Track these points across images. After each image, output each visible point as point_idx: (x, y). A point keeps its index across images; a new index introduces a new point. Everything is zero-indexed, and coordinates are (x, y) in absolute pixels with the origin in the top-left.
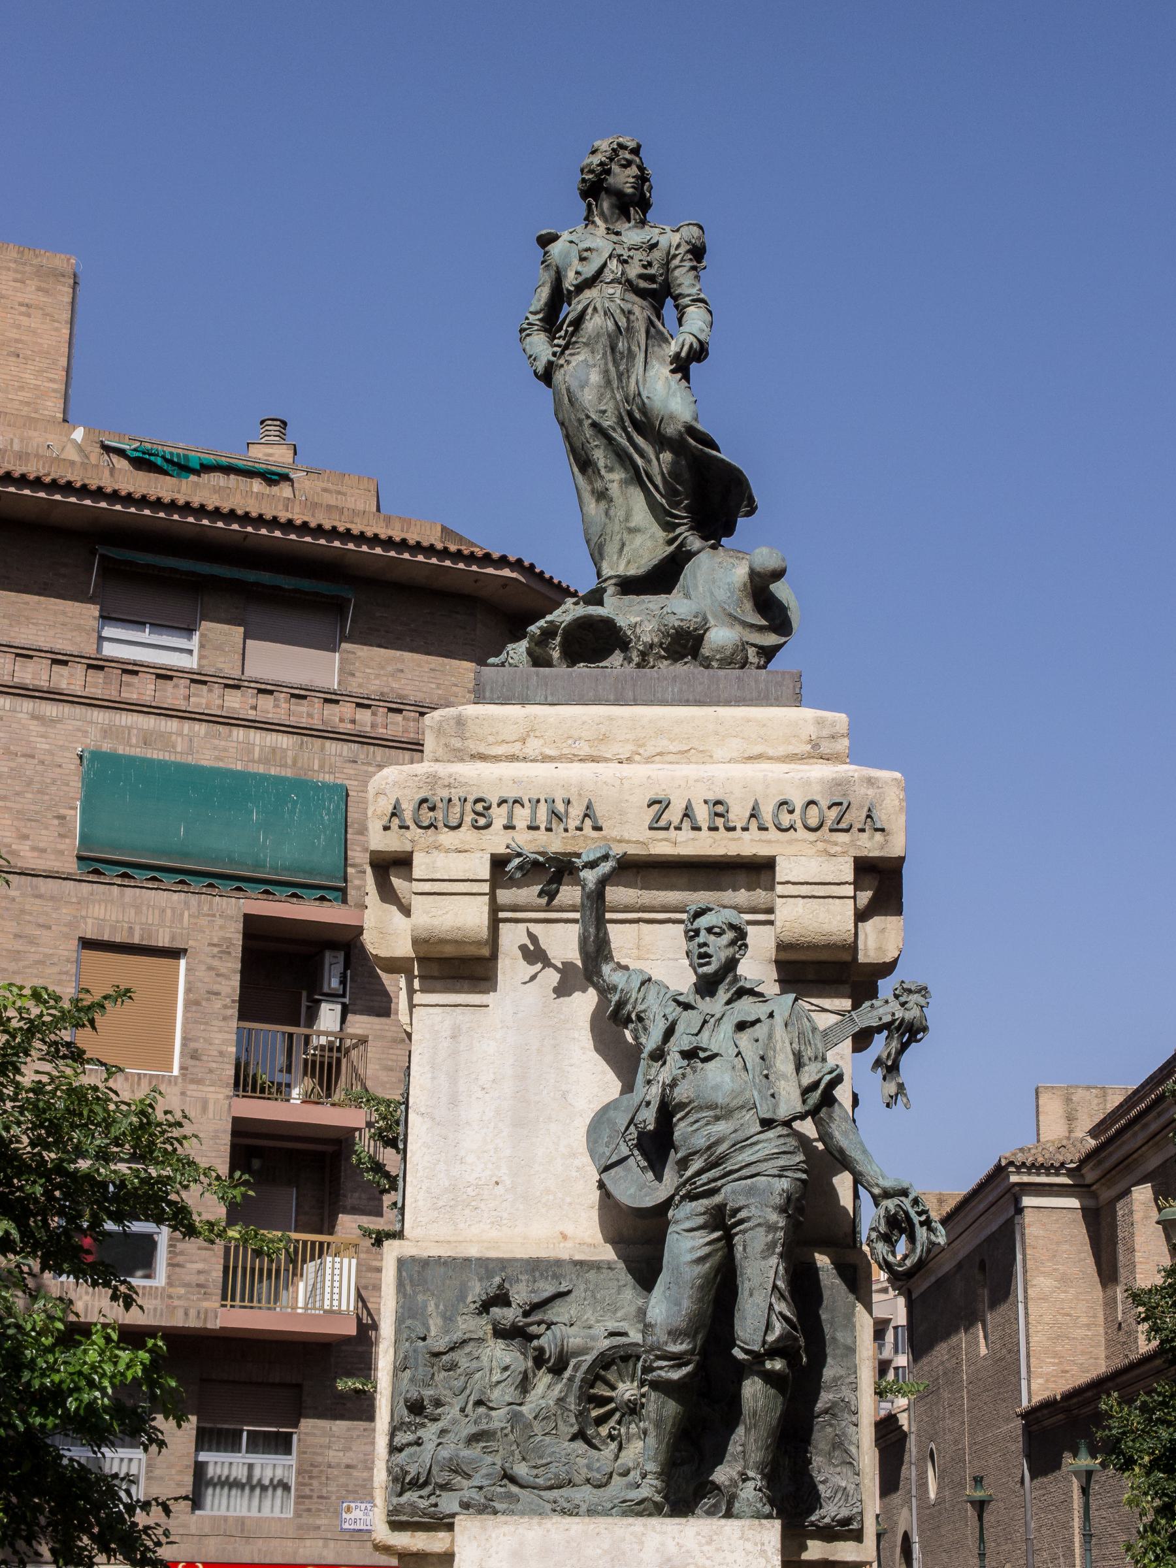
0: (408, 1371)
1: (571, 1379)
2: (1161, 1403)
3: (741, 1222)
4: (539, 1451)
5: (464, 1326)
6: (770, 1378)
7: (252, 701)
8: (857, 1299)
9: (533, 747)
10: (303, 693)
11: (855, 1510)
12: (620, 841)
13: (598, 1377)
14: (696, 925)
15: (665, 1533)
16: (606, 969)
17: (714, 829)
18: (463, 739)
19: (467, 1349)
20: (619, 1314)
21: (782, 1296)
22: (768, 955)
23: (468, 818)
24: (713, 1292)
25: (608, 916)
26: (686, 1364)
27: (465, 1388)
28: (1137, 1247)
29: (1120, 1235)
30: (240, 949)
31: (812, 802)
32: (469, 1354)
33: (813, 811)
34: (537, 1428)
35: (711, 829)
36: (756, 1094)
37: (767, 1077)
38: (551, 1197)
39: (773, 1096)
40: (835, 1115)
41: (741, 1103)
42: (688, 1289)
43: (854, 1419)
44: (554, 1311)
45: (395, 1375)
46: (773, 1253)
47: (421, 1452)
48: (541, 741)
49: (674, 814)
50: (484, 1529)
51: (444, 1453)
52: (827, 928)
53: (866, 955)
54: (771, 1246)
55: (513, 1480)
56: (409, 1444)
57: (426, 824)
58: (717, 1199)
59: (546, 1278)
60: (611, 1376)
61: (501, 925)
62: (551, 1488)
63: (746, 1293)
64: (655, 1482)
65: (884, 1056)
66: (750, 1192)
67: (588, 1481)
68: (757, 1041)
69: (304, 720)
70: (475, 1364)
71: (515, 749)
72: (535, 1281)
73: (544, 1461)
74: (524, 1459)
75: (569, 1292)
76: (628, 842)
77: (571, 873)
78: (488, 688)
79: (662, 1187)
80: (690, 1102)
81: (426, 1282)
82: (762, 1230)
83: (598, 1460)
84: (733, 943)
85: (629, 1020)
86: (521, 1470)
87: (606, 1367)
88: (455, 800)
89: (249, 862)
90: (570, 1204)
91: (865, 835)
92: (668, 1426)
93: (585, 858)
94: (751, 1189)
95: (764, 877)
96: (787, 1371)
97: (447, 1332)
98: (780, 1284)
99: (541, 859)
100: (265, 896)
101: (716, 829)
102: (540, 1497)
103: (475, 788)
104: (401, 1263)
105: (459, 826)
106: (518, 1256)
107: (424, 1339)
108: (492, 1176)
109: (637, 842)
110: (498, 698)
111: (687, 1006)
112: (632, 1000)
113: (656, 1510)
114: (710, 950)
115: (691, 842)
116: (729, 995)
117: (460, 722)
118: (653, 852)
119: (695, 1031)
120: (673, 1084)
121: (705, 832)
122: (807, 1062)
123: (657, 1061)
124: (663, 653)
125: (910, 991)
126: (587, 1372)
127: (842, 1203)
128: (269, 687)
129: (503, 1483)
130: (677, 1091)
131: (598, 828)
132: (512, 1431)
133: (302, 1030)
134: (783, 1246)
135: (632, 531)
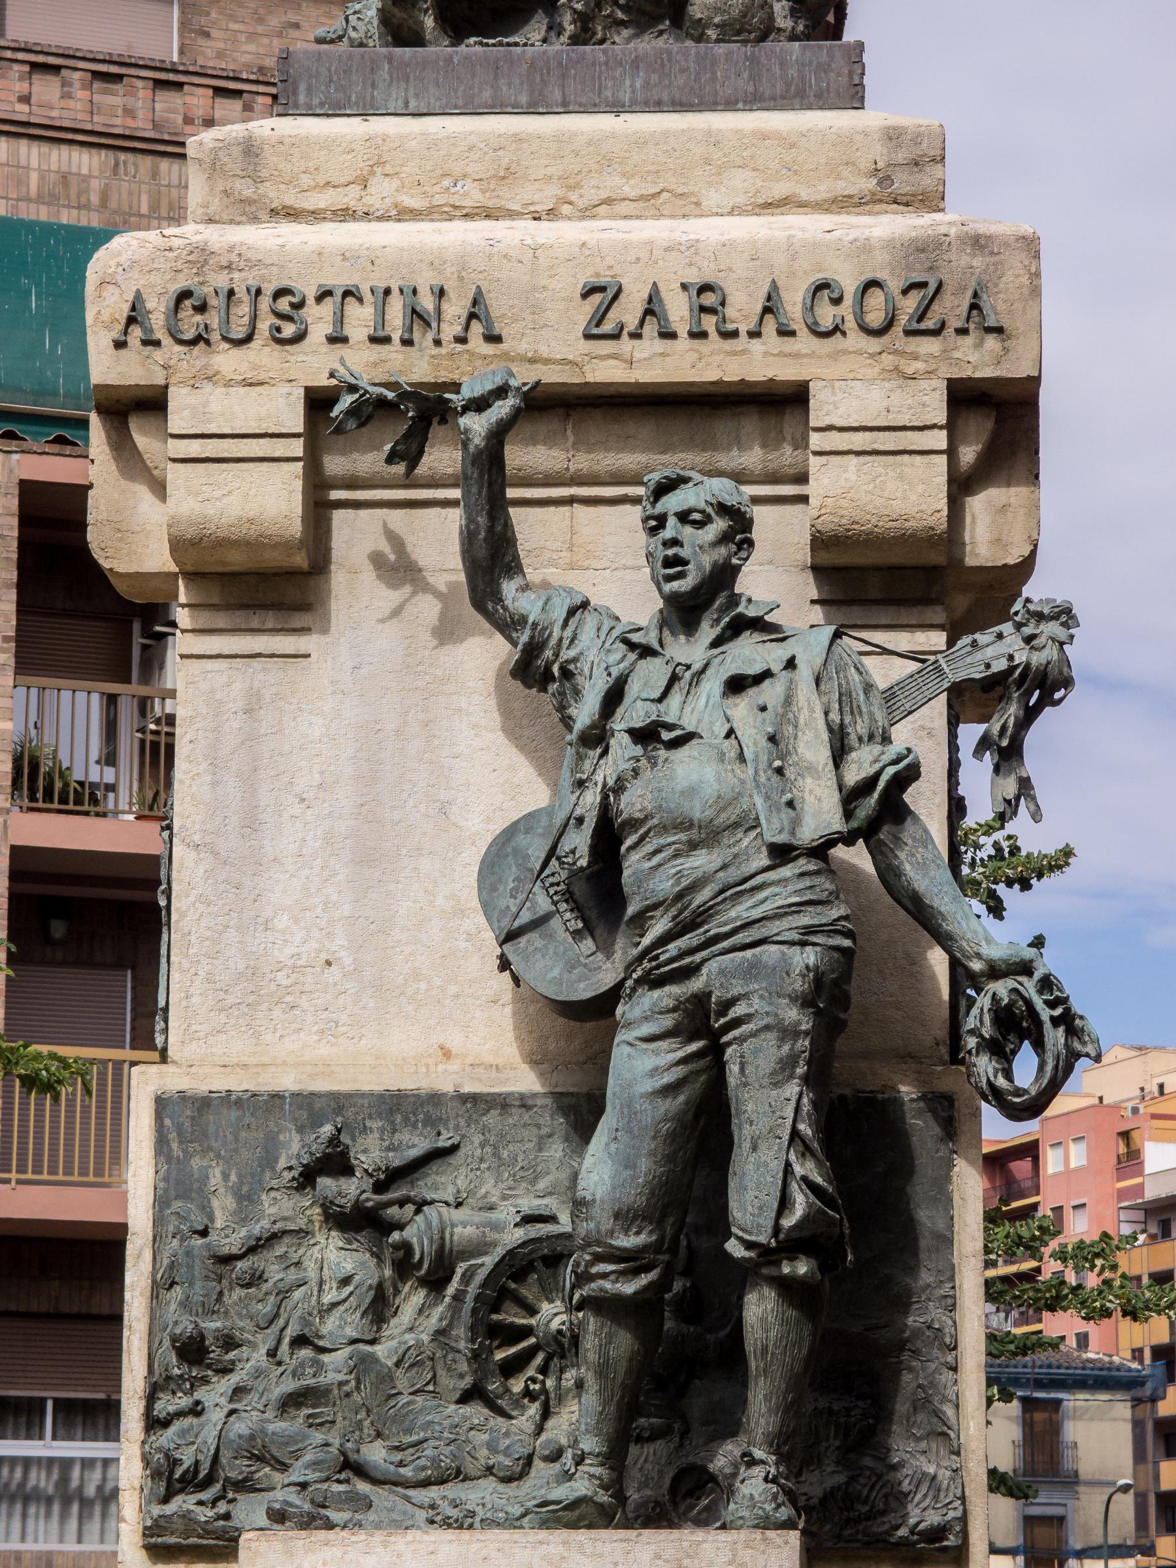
0: (177, 1288)
1: (458, 1297)
3: (737, 1023)
4: (404, 1421)
5: (273, 1210)
6: (788, 1288)
7: (22, 87)
9: (381, 193)
10: (114, 69)
11: (952, 1514)
12: (532, 361)
14: (659, 508)
15: (601, 1556)
16: (509, 588)
17: (699, 335)
18: (258, 181)
19: (279, 1250)
20: (542, 1185)
21: (807, 1150)
23: (265, 325)
25: (512, 493)
26: (647, 1269)
27: (277, 1316)
30: (15, 544)
31: (872, 284)
32: (283, 1257)
33: (876, 299)
34: (402, 1381)
36: (759, 801)
37: (780, 771)
38: (423, 986)
39: (790, 804)
40: (906, 837)
42: (648, 1140)
43: (950, 1359)
44: (429, 1181)
45: (155, 1296)
46: (792, 1076)
47: (202, 1425)
48: (395, 183)
49: (628, 312)
50: (289, 1553)
51: (240, 1427)
52: (899, 507)
54: (787, 1065)
55: (361, 1471)
56: (180, 1414)
57: (188, 336)
58: (696, 985)
59: (415, 1126)
60: (528, 1292)
62: (425, 1484)
63: (747, 1145)
64: (597, 1471)
66: (752, 970)
67: (489, 1470)
68: (763, 709)
69: (118, 121)
70: (292, 1275)
71: (349, 197)
72: (394, 1131)
73: (415, 1438)
75: (454, 1148)
76: (547, 361)
77: (443, 421)
78: (302, 87)
80: (646, 818)
81: (205, 1134)
82: (771, 1037)
83: (507, 1434)
84: (725, 538)
86: (376, 1454)
87: (520, 1275)
88: (241, 292)
89: (27, 386)
91: (969, 340)
93: (467, 393)
96: (908, 1280)
97: (243, 1221)
99: (390, 395)
100: (56, 448)
101: (703, 335)
102: (408, 1499)
103: (275, 270)
104: (161, 1104)
105: (248, 339)
106: (366, 1088)
107: (204, 1233)
108: (319, 951)
109: (564, 362)
110: (322, 105)
111: (646, 652)
112: (553, 642)
114: (684, 553)
115: (659, 360)
116: (718, 630)
117: (250, 150)
118: (590, 378)
119: (657, 694)
120: (619, 787)
121: (683, 343)
124: (620, 15)
125: (1040, 617)
126: (484, 1285)
128: (52, 60)
129: (343, 1476)
130: (625, 798)
131: (493, 338)
132: (358, 1388)
133: (135, 688)
134: (809, 1063)
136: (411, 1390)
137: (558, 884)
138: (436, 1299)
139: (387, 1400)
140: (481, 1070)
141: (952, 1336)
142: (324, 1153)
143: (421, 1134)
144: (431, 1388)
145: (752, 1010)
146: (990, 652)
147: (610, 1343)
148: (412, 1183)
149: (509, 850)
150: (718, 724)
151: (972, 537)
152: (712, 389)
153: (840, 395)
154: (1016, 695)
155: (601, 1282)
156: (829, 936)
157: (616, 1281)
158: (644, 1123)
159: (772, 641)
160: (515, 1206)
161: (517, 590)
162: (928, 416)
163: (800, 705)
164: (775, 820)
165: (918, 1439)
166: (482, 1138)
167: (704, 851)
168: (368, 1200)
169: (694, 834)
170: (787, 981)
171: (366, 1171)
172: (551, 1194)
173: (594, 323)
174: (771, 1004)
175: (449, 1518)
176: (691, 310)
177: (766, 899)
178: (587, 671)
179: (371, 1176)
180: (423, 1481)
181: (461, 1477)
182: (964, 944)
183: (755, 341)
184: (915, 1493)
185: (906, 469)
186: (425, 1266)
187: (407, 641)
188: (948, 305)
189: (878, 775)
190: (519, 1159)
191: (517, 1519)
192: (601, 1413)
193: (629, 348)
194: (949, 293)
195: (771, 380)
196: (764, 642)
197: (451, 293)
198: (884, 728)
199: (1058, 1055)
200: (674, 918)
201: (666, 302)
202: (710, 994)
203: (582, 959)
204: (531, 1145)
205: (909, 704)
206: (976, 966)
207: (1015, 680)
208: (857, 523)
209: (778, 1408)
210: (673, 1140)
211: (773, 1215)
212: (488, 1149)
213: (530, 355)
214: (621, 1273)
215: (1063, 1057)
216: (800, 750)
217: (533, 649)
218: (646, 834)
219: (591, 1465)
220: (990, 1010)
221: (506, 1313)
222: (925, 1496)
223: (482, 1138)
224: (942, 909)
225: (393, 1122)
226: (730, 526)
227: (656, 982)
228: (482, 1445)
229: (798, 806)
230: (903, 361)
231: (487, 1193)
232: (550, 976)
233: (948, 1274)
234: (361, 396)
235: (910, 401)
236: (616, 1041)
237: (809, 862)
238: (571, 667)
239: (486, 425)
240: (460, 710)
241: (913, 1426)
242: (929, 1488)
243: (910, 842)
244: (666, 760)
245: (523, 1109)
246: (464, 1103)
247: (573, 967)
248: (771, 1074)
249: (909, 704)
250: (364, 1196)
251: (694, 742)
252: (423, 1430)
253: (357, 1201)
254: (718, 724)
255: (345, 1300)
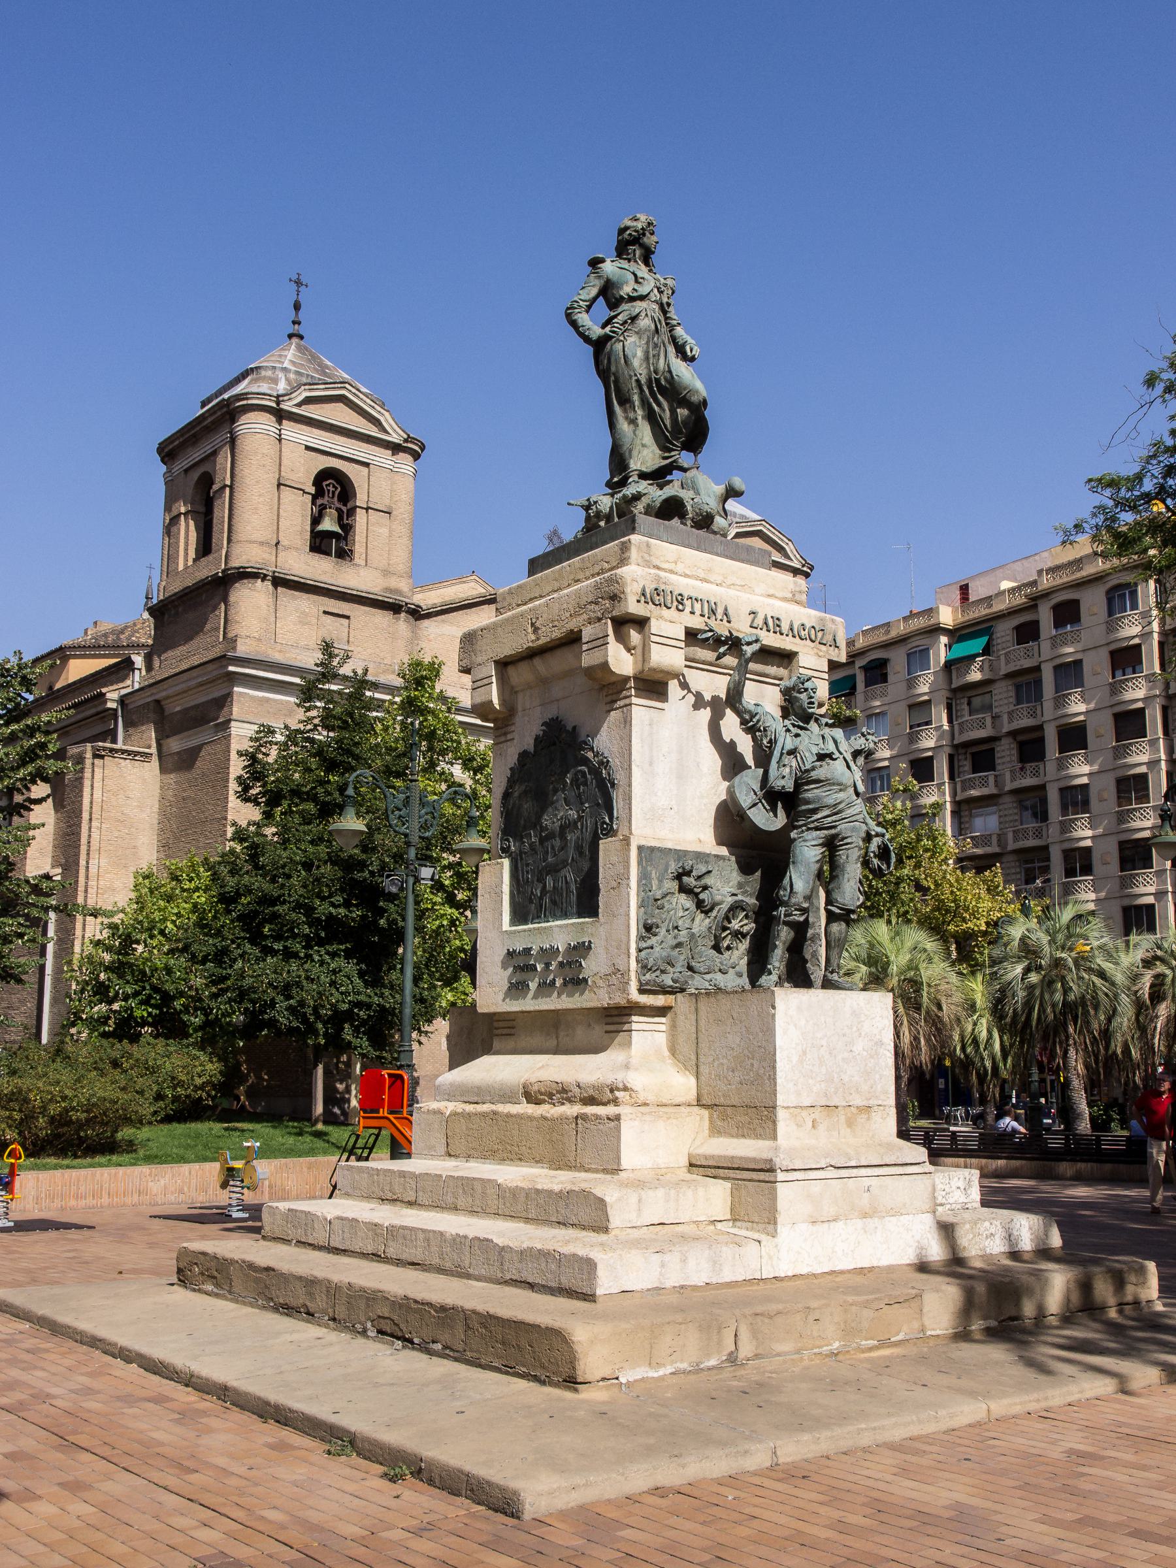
17: (775, 632)
18: (650, 555)
19: (668, 898)
58: (833, 831)
91: (832, 648)
95: (786, 661)
97: (660, 888)
131: (729, 622)
135: (644, 446)
197: (718, 604)
206: (873, 833)
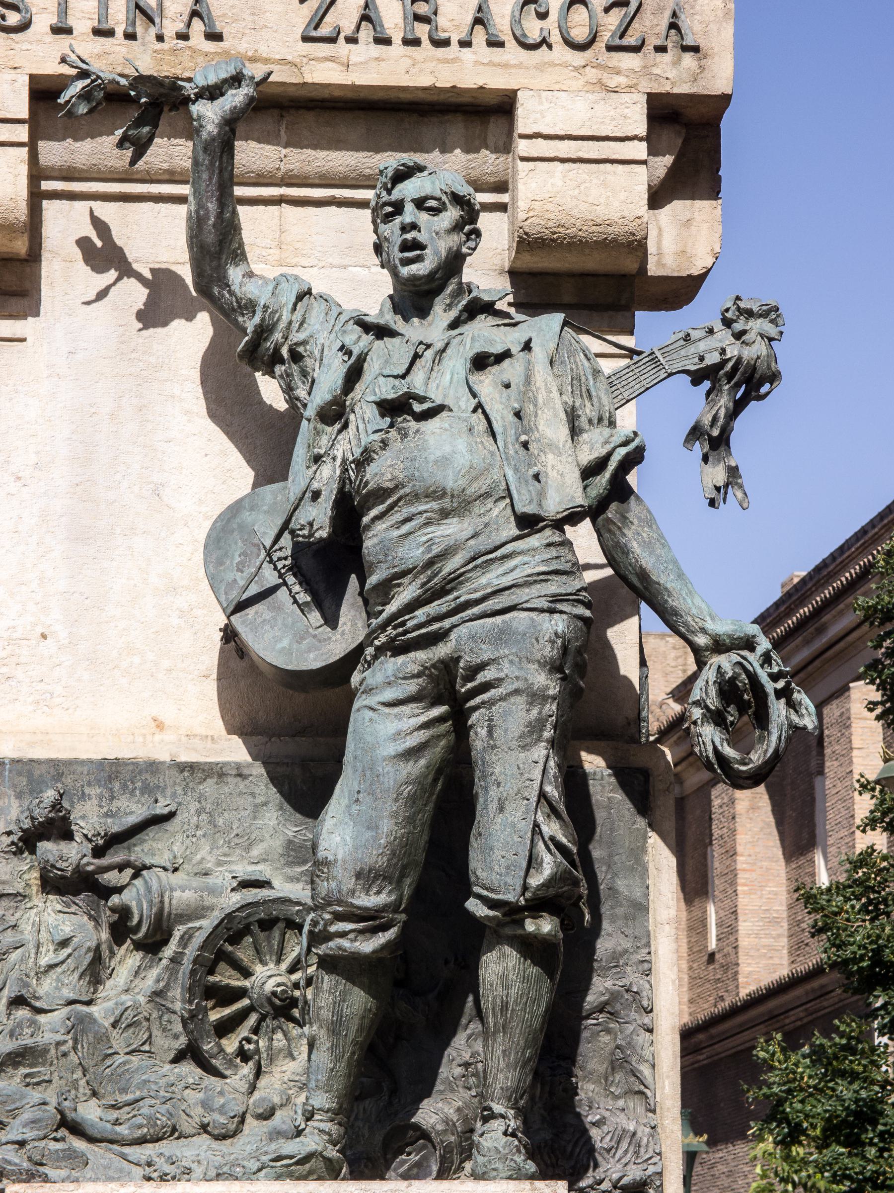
1: (175, 960)
2: (843, 1048)
3: (486, 687)
8: (650, 825)
11: (651, 1169)
13: (222, 956)
14: (396, 194)
16: (235, 274)
17: (412, 42)
20: (255, 852)
21: (554, 811)
22: (497, 261)
24: (430, 807)
26: (384, 928)
28: (739, 849)
29: (716, 832)
34: (118, 1040)
35: (407, 42)
36: (510, 474)
37: (525, 445)
38: (137, 660)
40: (631, 516)
41: (484, 489)
42: (390, 801)
43: (647, 1020)
44: (146, 847)
46: (539, 739)
52: (602, 213)
53: (659, 263)
54: (536, 727)
55: (77, 1129)
58: (442, 650)
59: (132, 793)
60: (244, 953)
61: (45, 203)
62: (141, 1141)
63: (493, 806)
64: (327, 1126)
65: (707, 420)
66: (501, 637)
67: (204, 1128)
68: (508, 386)
72: (112, 798)
73: (130, 1097)
74: (95, 1094)
75: (171, 815)
77: (174, 107)
79: (337, 636)
80: (397, 487)
83: (221, 1093)
84: (457, 227)
85: (276, 358)
87: (235, 939)
90: (169, 671)
91: (667, 58)
92: (352, 1030)
93: (201, 82)
94: (502, 632)
95: (495, 127)
98: (551, 790)
102: (124, 1157)
106: (84, 756)
111: (382, 332)
112: (282, 325)
113: (332, 1172)
115: (374, 64)
116: (454, 313)
118: (309, 79)
119: (401, 370)
120: (365, 459)
121: (397, 48)
122: (586, 426)
123: (331, 424)
125: (749, 314)
126: (202, 948)
127: (623, 671)
129: (59, 1135)
130: (370, 471)
131: (214, 36)
132: (75, 1048)
134: (555, 728)
136: (127, 1050)
137: (286, 558)
138: (152, 960)
139: (103, 1060)
140: (196, 740)
141: (649, 999)
142: (47, 817)
143: (139, 802)
144: (146, 1048)
145: (502, 675)
146: (702, 346)
147: (344, 1001)
148: (129, 849)
149: (235, 526)
150: (464, 399)
151: (659, 248)
152: (422, 96)
153: (546, 105)
154: (727, 387)
155: (339, 941)
156: (574, 606)
157: (355, 940)
158: (387, 786)
159: (505, 325)
160: (230, 872)
161: (244, 276)
162: (630, 128)
163: (538, 385)
164: (524, 491)
165: (617, 1097)
166: (198, 806)
167: (455, 520)
168: (88, 864)
169: (446, 503)
170: (537, 647)
171: (86, 836)
172: (264, 860)
173: (313, 25)
174: (521, 669)
175: (166, 1175)
176: (405, 18)
177: (516, 567)
178: (317, 353)
179: (90, 841)
180: (139, 1138)
181: (176, 1135)
182: (689, 619)
183: (466, 50)
184: (617, 1148)
185: (609, 177)
186: (144, 929)
187: (121, 329)
188: (648, 23)
189: (609, 455)
190: (234, 827)
191: (254, 1173)
192: (332, 1070)
193: (346, 52)
194: (648, 12)
195: (481, 88)
196: (498, 325)
198: (610, 413)
199: (782, 725)
200: (423, 585)
201: (380, 9)
202: (459, 657)
203: (311, 630)
204: (247, 813)
205: (627, 393)
207: (726, 374)
208: (563, 226)
209: (517, 1063)
210: (414, 803)
211: (522, 874)
212: (204, 817)
213: (250, 54)
214: (361, 932)
215: (785, 728)
216: (540, 428)
217: (262, 331)
218: (395, 504)
219: (321, 1121)
220: (715, 682)
221: (221, 974)
222: (626, 1152)
223: (198, 806)
224: (668, 586)
225: (111, 789)
226: (461, 216)
227: (398, 648)
228: (196, 1104)
229: (543, 480)
230: (605, 74)
231: (203, 859)
232: (279, 646)
233: (644, 941)
234: (93, 81)
235: (612, 113)
236: (356, 706)
237: (554, 533)
238: (301, 349)
239: (220, 112)
240: (173, 396)
241: (611, 1085)
242: (630, 1144)
243: (636, 521)
244: (417, 431)
245: (239, 779)
246: (182, 771)
247: (302, 638)
248: (520, 737)
249: (627, 393)
250: (85, 860)
251: (444, 414)
252: (139, 1089)
253: (78, 866)
254: (464, 399)
255: (62, 962)
